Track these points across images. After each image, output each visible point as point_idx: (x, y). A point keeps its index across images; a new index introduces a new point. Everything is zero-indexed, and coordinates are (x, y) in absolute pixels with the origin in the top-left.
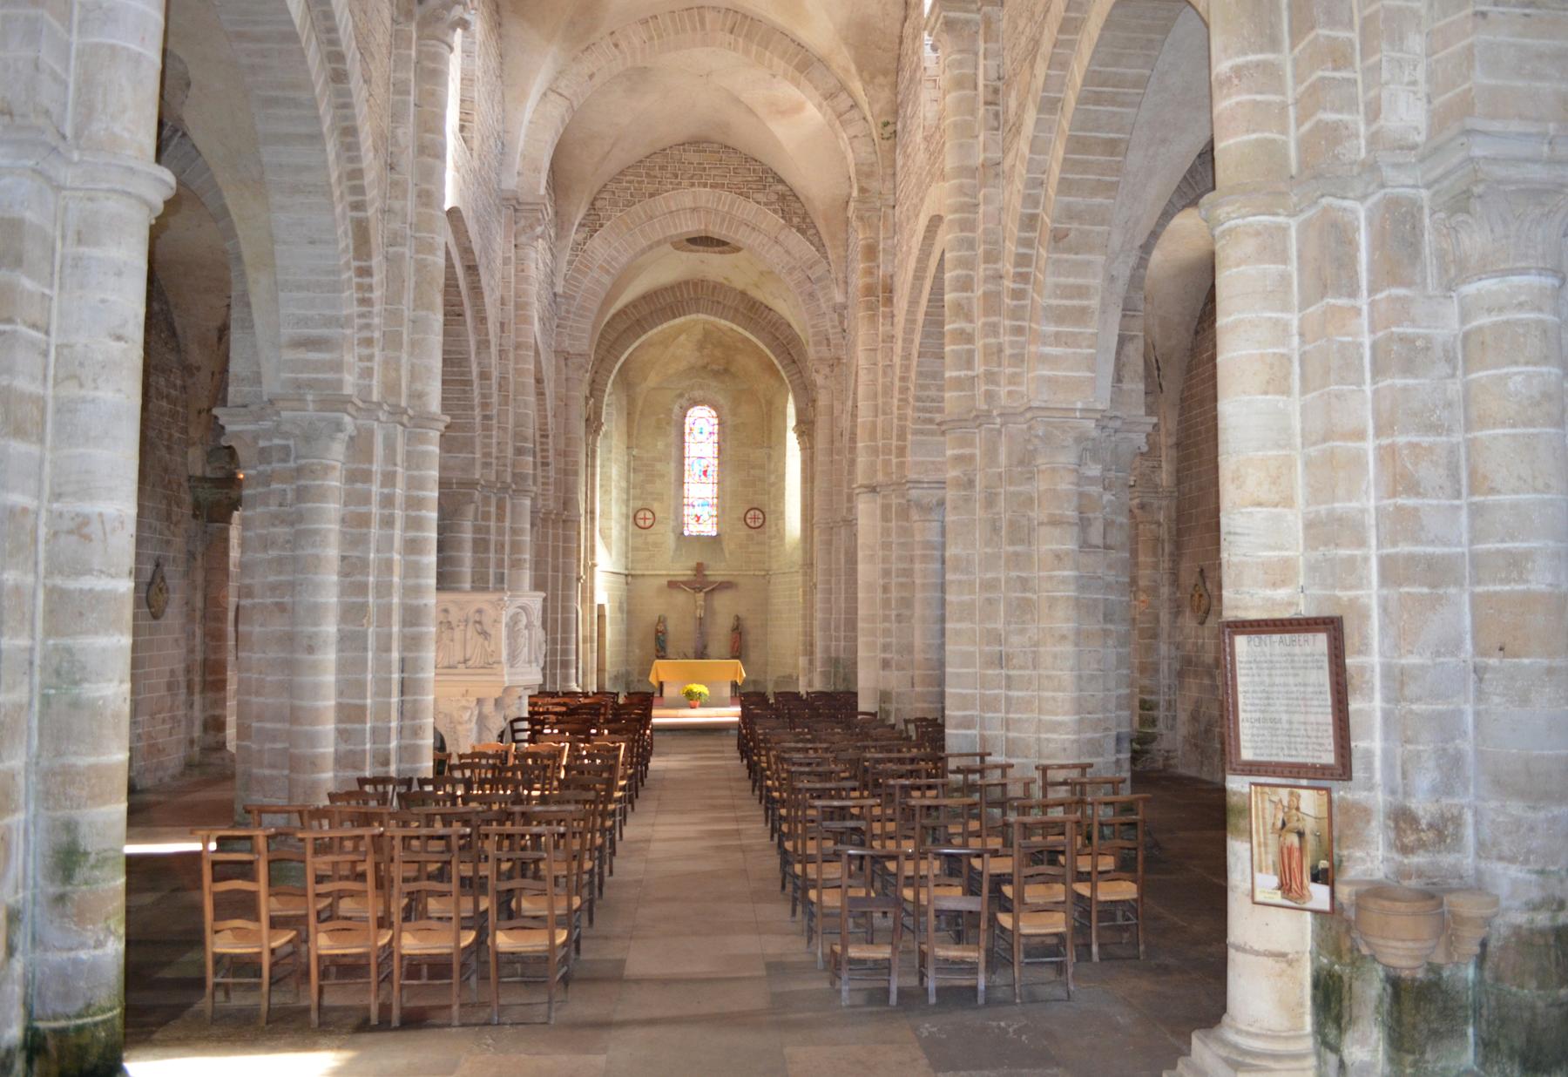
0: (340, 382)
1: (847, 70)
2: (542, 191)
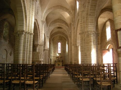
0: (23, 29)
1: (70, 10)
2: (45, 20)
